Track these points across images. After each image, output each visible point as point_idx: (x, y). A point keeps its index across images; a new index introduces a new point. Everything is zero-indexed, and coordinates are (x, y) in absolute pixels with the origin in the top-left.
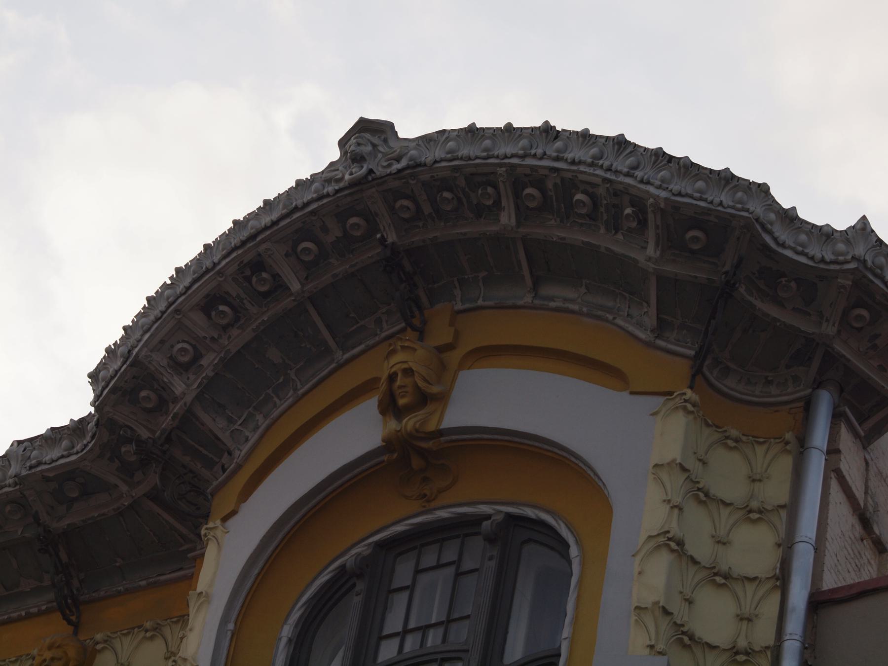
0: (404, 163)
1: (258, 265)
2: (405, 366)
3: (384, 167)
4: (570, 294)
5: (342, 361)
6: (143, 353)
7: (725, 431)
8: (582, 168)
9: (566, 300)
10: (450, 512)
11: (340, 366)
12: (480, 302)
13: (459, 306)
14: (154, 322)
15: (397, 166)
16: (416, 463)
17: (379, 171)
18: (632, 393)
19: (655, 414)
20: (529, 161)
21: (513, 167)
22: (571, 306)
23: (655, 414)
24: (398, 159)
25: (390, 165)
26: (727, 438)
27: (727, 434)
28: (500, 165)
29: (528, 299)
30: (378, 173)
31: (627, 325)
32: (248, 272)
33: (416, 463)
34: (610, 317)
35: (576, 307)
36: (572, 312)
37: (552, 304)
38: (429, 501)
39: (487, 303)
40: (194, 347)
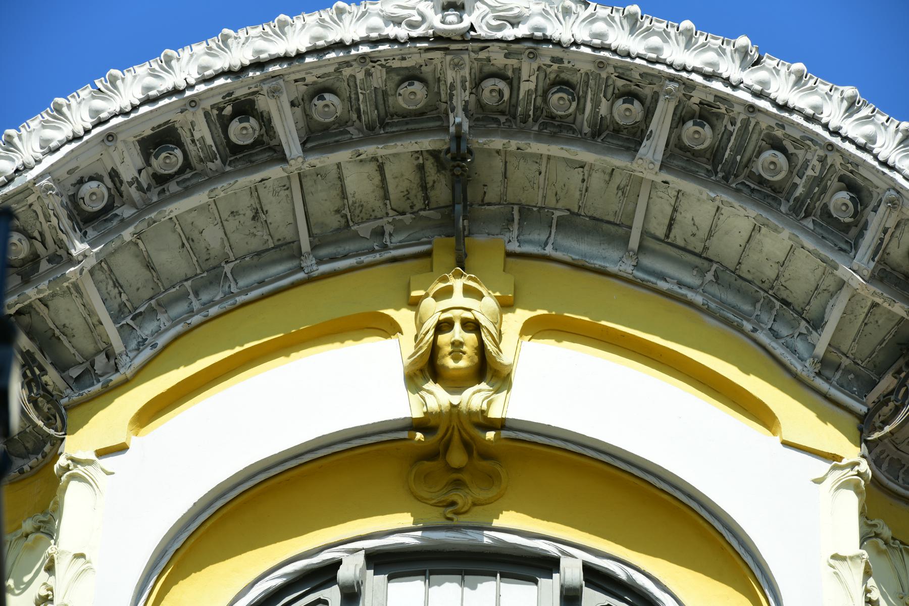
0: (522, 31)
1: (244, 108)
2: (468, 315)
3: (491, 27)
4: (688, 278)
5: (316, 274)
6: (44, 182)
7: (875, 526)
8: (796, 118)
9: (680, 284)
10: (557, 548)
11: (310, 280)
12: (549, 250)
13: (514, 247)
14: (69, 141)
15: (510, 33)
16: (457, 458)
17: (483, 32)
18: (786, 444)
19: (818, 481)
20: (717, 85)
21: (690, 86)
22: (690, 295)
23: (818, 481)
24: (514, 22)
25: (500, 28)
26: (877, 535)
27: (878, 530)
28: (672, 79)
29: (626, 268)
30: (479, 32)
31: (774, 344)
32: (228, 110)
33: (457, 458)
34: (748, 326)
35: (699, 299)
36: (690, 304)
37: (662, 285)
38: (457, 513)
39: (559, 255)
40: (110, 195)
